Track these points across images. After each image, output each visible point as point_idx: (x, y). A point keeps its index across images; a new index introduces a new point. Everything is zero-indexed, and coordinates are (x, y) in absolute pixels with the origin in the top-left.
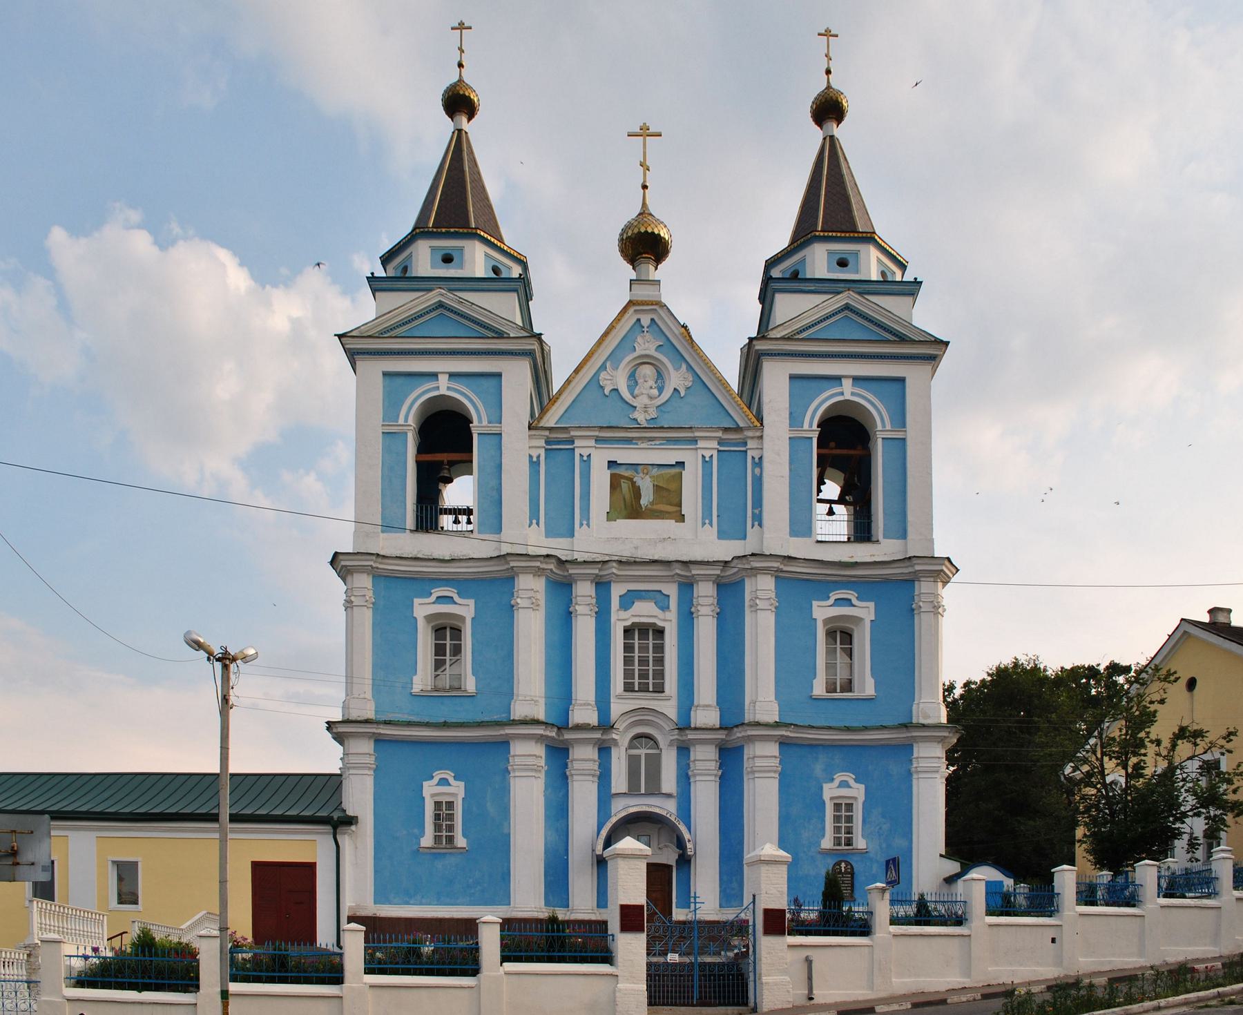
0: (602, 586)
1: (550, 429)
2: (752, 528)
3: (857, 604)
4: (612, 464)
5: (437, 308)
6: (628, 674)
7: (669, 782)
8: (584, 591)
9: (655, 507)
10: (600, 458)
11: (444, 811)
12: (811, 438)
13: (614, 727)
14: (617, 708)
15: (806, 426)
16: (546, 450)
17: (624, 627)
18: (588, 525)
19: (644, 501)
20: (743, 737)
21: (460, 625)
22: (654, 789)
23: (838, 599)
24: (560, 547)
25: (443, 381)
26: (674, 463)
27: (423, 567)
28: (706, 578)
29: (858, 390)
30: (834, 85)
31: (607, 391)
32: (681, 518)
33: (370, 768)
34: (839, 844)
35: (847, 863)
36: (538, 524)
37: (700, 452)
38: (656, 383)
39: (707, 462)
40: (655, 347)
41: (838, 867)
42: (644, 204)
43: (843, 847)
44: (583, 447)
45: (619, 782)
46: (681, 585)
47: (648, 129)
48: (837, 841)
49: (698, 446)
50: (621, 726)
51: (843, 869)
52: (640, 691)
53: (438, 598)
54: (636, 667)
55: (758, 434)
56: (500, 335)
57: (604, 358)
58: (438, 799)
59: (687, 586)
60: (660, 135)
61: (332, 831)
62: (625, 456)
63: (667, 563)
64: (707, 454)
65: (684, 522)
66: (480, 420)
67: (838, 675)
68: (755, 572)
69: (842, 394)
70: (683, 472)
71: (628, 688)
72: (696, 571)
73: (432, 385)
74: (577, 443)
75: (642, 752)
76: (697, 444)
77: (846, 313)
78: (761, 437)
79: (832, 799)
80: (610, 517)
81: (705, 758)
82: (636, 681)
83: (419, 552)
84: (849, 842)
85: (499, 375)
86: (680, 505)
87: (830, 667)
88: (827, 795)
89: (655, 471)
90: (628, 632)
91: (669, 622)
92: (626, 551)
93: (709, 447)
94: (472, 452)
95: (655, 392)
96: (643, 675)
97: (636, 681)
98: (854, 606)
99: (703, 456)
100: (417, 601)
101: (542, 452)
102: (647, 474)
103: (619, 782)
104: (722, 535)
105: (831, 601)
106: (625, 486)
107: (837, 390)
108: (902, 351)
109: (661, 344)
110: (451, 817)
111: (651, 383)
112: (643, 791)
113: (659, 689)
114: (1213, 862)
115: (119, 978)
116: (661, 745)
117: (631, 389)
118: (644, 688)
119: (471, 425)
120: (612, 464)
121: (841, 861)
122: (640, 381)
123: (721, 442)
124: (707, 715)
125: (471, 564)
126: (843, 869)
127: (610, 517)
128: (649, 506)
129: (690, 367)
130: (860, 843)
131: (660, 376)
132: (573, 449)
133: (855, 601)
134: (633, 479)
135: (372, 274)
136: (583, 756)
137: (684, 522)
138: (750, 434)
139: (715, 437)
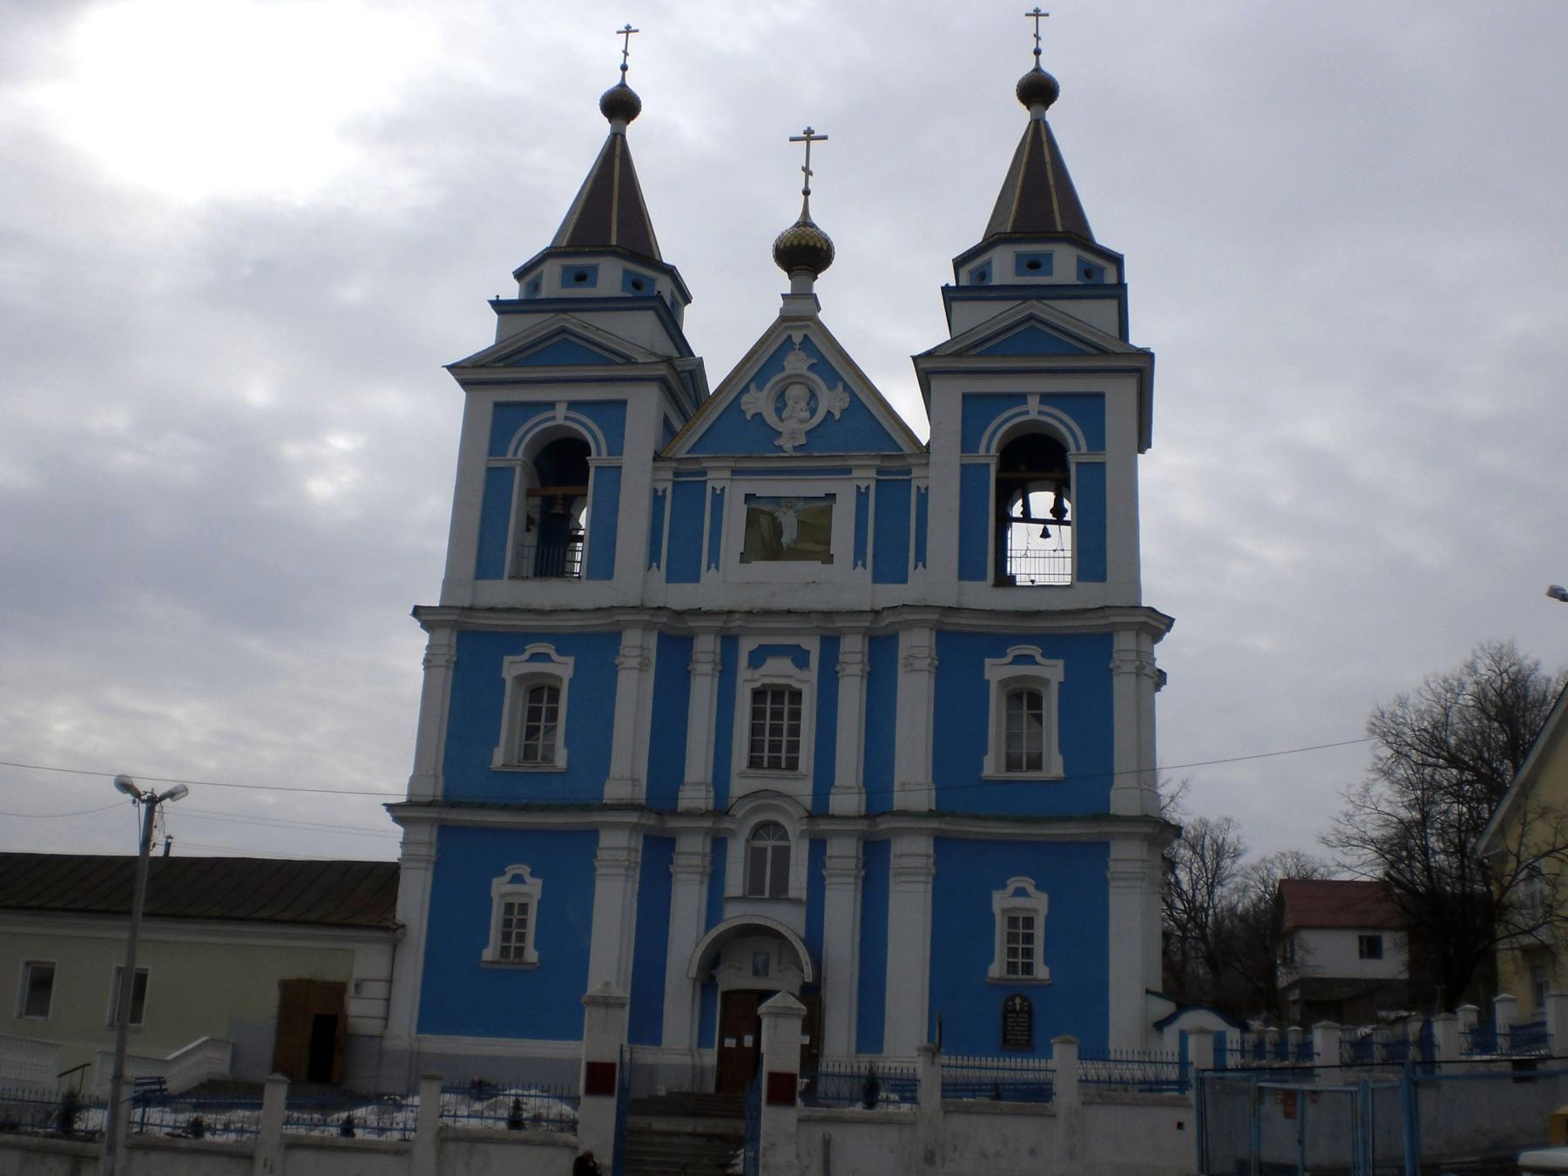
0: (729, 642)
1: (680, 460)
2: (915, 569)
3: (1040, 662)
4: (749, 497)
6: (755, 746)
8: (706, 647)
11: (516, 916)
12: (988, 465)
13: (730, 813)
14: (739, 786)
15: (982, 450)
16: (877, 481)
17: (752, 689)
18: (717, 568)
19: (786, 540)
20: (887, 829)
21: (1042, 690)
22: (779, 891)
24: (681, 596)
25: (561, 412)
26: (824, 496)
27: (563, 620)
28: (853, 631)
29: (1045, 408)
31: (748, 417)
32: (828, 559)
33: (849, 876)
34: (1015, 972)
36: (658, 567)
37: (855, 483)
38: (808, 404)
39: (862, 493)
41: (1011, 1003)
42: (806, 212)
43: (1021, 976)
45: (735, 878)
47: (813, 133)
48: (1012, 967)
49: (708, 477)
50: (739, 812)
51: (1018, 1007)
52: (770, 767)
54: (767, 737)
55: (924, 461)
56: (629, 361)
57: (747, 380)
58: (510, 900)
59: (830, 644)
62: (767, 488)
63: (805, 614)
64: (863, 485)
65: (832, 563)
66: (599, 453)
68: (910, 626)
70: (834, 505)
71: (754, 763)
72: (693, 623)
74: (711, 475)
75: (769, 844)
77: (1033, 323)
79: (1004, 911)
80: (744, 558)
81: (843, 853)
82: (766, 754)
85: (623, 403)
86: (828, 543)
87: (1012, 738)
89: (800, 505)
90: (758, 695)
91: (807, 682)
92: (760, 601)
95: (807, 414)
96: (775, 747)
97: (766, 754)
98: (1039, 664)
100: (507, 659)
101: (669, 486)
103: (735, 878)
104: (878, 578)
105: (1009, 658)
106: (764, 522)
109: (815, 361)
110: (522, 923)
111: (803, 405)
112: (767, 895)
113: (793, 765)
116: (791, 836)
117: (779, 411)
118: (774, 764)
119: (588, 458)
120: (749, 497)
122: (790, 402)
124: (847, 799)
125: (573, 616)
126: (1018, 1007)
127: (744, 558)
128: (792, 545)
129: (846, 387)
130: (1042, 972)
132: (910, 480)
133: (1039, 658)
134: (773, 514)
136: (691, 850)
137: (832, 563)
139: (726, 467)
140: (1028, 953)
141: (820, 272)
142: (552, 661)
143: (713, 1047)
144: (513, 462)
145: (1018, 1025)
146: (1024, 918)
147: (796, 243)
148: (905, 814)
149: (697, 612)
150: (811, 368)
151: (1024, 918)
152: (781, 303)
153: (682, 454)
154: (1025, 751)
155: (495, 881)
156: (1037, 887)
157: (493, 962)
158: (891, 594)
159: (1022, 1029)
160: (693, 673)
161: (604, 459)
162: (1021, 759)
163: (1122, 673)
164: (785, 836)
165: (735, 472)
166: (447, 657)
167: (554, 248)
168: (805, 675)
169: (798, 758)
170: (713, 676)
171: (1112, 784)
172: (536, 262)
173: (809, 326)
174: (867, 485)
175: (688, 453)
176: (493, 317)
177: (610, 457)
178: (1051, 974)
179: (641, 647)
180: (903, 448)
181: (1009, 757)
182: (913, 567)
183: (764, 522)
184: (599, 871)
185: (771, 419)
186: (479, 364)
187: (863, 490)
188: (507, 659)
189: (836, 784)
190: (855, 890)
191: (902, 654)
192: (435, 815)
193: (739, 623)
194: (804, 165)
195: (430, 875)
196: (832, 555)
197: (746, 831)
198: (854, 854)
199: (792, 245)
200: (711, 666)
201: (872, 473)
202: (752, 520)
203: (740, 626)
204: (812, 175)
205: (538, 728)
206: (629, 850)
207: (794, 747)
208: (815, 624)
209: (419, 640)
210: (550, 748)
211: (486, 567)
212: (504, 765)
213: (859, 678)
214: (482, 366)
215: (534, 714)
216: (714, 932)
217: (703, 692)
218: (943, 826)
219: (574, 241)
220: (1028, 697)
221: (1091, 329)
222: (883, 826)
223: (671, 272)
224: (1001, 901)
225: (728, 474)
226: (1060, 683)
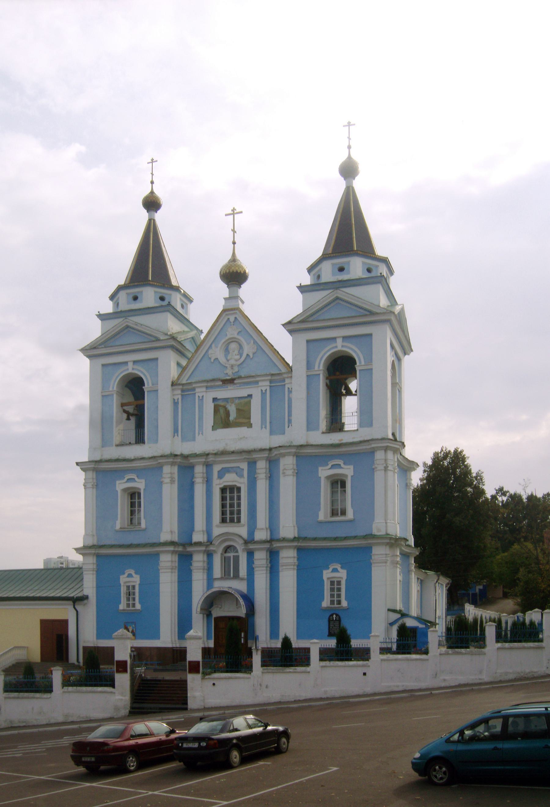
0: (208, 466)
1: (183, 385)
2: (288, 427)
4: (215, 399)
5: (126, 328)
6: (223, 513)
7: (243, 571)
8: (199, 470)
9: (237, 421)
10: (209, 396)
12: (319, 374)
13: (212, 543)
15: (316, 368)
18: (202, 434)
19: (232, 417)
22: (236, 576)
23: (334, 465)
24: (186, 448)
28: (261, 459)
30: (354, 156)
31: (212, 360)
32: (250, 426)
33: (263, 567)
35: (337, 615)
36: (178, 435)
37: (260, 389)
40: (237, 332)
41: (331, 617)
44: (200, 392)
45: (217, 572)
46: (249, 463)
48: (332, 602)
49: (258, 385)
50: (216, 542)
53: (128, 479)
54: (228, 509)
55: (290, 375)
56: (158, 340)
58: (128, 584)
59: (252, 464)
60: (344, 126)
61: (73, 604)
67: (339, 505)
68: (284, 455)
69: (336, 347)
70: (252, 400)
71: (223, 521)
72: (192, 460)
73: (125, 368)
75: (231, 555)
76: (258, 384)
77: (338, 301)
78: (291, 377)
79: (328, 578)
80: (214, 428)
81: (261, 557)
83: (119, 456)
84: (339, 602)
85: (370, 335)
86: (249, 418)
88: (325, 578)
90: (223, 490)
91: (243, 483)
92: (220, 447)
93: (265, 385)
94: (144, 399)
95: (238, 357)
99: (261, 390)
100: (118, 482)
101: (180, 397)
102: (233, 403)
103: (217, 572)
104: (272, 433)
106: (222, 411)
107: (334, 345)
108: (110, 466)
109: (240, 330)
111: (236, 352)
113: (239, 521)
114: (371, 638)
115: (446, 587)
116: (239, 551)
117: (226, 356)
118: (232, 521)
119: (143, 387)
120: (215, 399)
121: (332, 615)
122: (231, 351)
123: (271, 381)
125: (142, 461)
127: (214, 428)
130: (344, 604)
131: (241, 347)
135: (99, 312)
136: (199, 560)
138: (285, 376)
140: (339, 596)
141: (242, 284)
142: (136, 481)
143: (212, 639)
144: (113, 392)
145: (334, 626)
146: (337, 581)
147: (228, 271)
148: (284, 540)
149: (196, 456)
150: (239, 333)
151: (337, 581)
152: (223, 302)
153: (184, 382)
154: (339, 508)
155: (121, 577)
156: (342, 568)
157: (122, 610)
158: (277, 440)
159: (336, 627)
160: (257, 478)
161: (316, 371)
162: (338, 511)
163: (378, 470)
164: (237, 552)
165: (207, 387)
166: (92, 483)
167: (325, 255)
168: (242, 480)
169: (241, 517)
170: (203, 483)
171: (374, 520)
172: (314, 265)
173: (236, 313)
174: (265, 389)
175: (187, 380)
176: (99, 322)
177: (153, 386)
178: (348, 604)
179: (171, 473)
180: (281, 369)
181: (333, 510)
182: (287, 427)
183: (222, 411)
184: (161, 571)
185: (222, 360)
186: (92, 347)
187: (264, 392)
188: (118, 482)
189: (257, 527)
190: (266, 573)
191: (281, 467)
192: (94, 552)
193: (211, 459)
194: (233, 229)
195: (95, 576)
196: (252, 424)
197: (220, 550)
198: (265, 557)
199: (226, 272)
200: (264, 475)
201: (268, 383)
202: (216, 410)
203: (212, 460)
204: (236, 233)
205: (135, 511)
206: (172, 561)
207: (239, 512)
208: (244, 457)
209: (80, 476)
210: (139, 519)
211: (105, 443)
212: (121, 528)
213: (264, 480)
214: (95, 348)
215: (132, 505)
216: (209, 592)
217: (199, 490)
218: (299, 544)
219: (130, 282)
220: (229, 490)
221: (363, 301)
222: (275, 546)
223: (385, 261)
224: (327, 574)
225: (204, 389)
226: (352, 476)
